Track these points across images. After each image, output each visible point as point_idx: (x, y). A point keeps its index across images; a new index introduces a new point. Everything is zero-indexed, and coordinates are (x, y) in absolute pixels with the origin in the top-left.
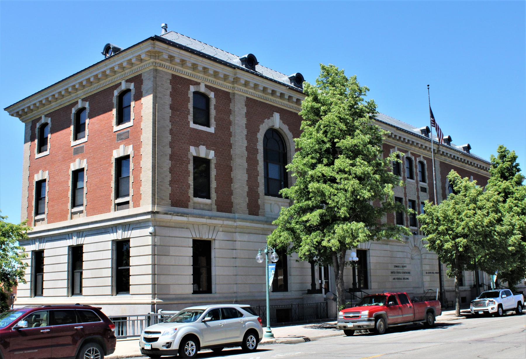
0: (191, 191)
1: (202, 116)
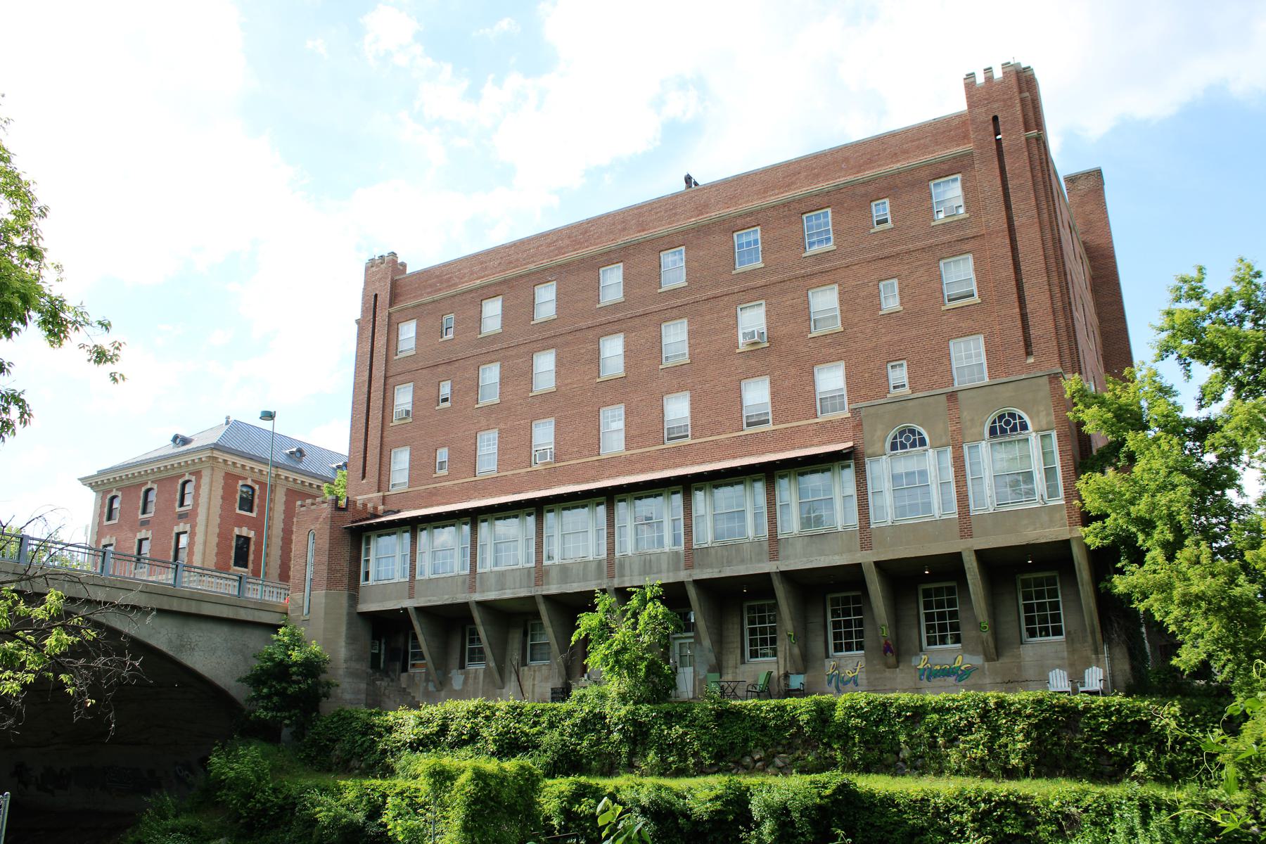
0: (232, 562)
1: (247, 503)
